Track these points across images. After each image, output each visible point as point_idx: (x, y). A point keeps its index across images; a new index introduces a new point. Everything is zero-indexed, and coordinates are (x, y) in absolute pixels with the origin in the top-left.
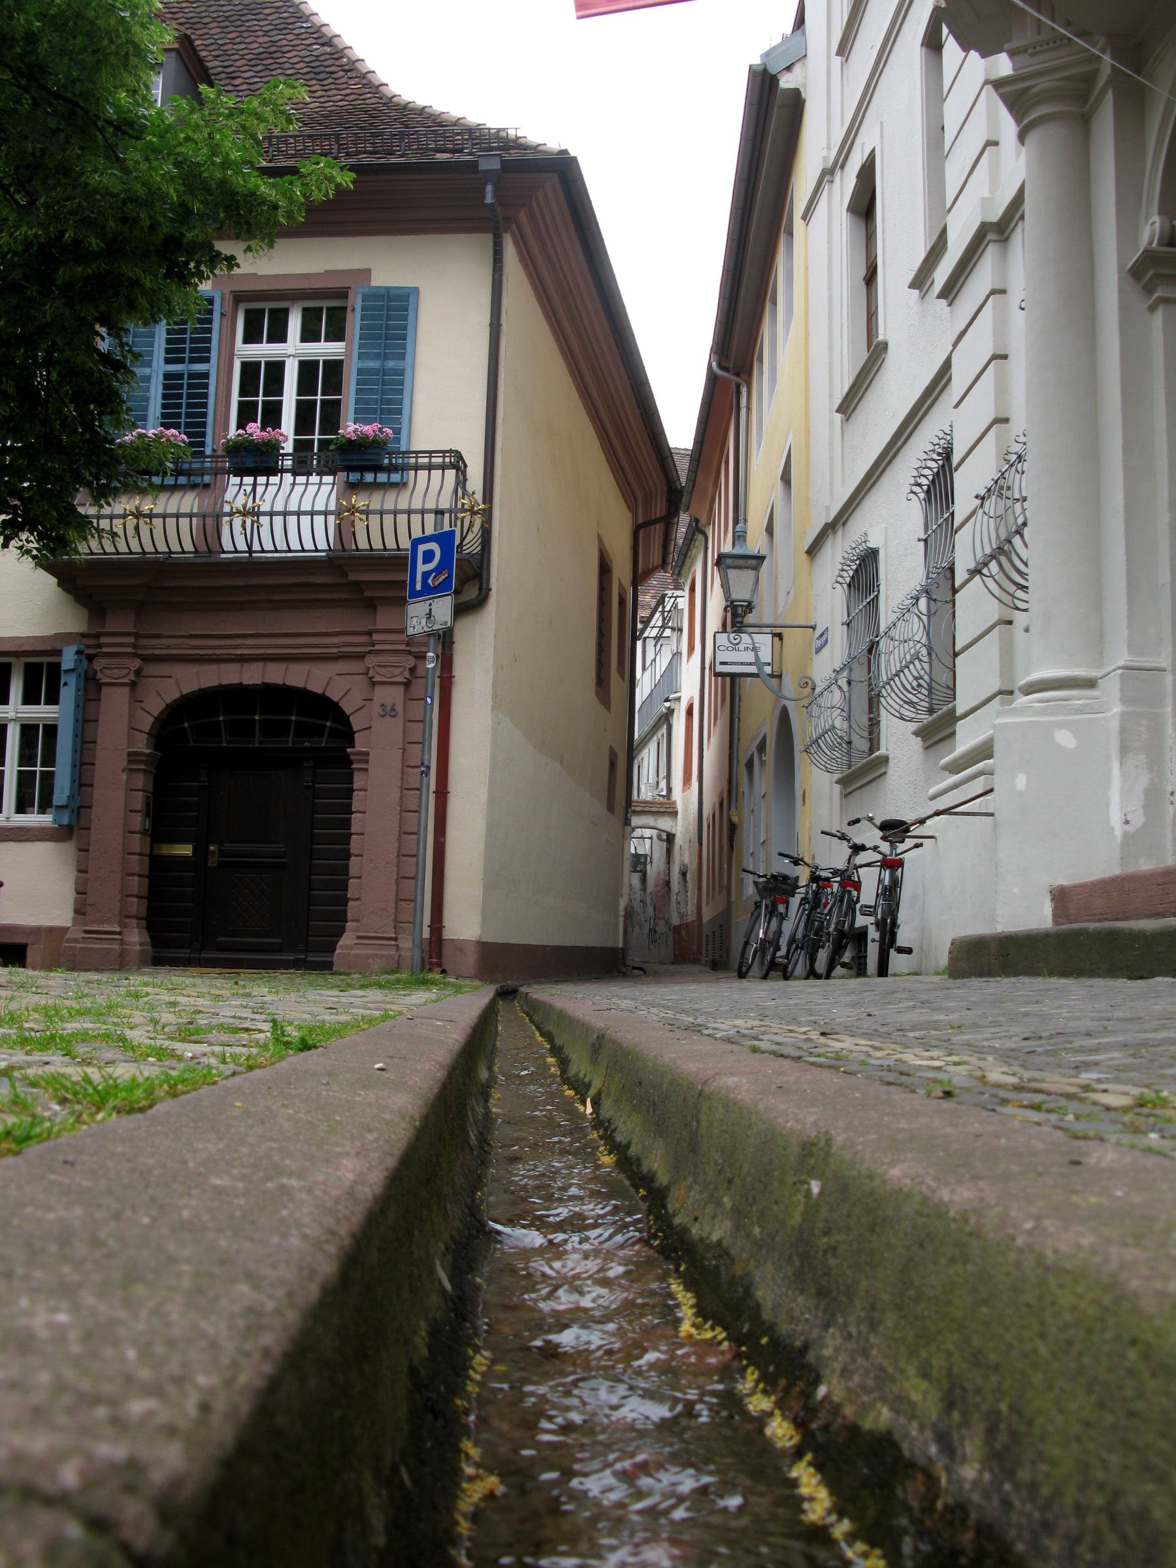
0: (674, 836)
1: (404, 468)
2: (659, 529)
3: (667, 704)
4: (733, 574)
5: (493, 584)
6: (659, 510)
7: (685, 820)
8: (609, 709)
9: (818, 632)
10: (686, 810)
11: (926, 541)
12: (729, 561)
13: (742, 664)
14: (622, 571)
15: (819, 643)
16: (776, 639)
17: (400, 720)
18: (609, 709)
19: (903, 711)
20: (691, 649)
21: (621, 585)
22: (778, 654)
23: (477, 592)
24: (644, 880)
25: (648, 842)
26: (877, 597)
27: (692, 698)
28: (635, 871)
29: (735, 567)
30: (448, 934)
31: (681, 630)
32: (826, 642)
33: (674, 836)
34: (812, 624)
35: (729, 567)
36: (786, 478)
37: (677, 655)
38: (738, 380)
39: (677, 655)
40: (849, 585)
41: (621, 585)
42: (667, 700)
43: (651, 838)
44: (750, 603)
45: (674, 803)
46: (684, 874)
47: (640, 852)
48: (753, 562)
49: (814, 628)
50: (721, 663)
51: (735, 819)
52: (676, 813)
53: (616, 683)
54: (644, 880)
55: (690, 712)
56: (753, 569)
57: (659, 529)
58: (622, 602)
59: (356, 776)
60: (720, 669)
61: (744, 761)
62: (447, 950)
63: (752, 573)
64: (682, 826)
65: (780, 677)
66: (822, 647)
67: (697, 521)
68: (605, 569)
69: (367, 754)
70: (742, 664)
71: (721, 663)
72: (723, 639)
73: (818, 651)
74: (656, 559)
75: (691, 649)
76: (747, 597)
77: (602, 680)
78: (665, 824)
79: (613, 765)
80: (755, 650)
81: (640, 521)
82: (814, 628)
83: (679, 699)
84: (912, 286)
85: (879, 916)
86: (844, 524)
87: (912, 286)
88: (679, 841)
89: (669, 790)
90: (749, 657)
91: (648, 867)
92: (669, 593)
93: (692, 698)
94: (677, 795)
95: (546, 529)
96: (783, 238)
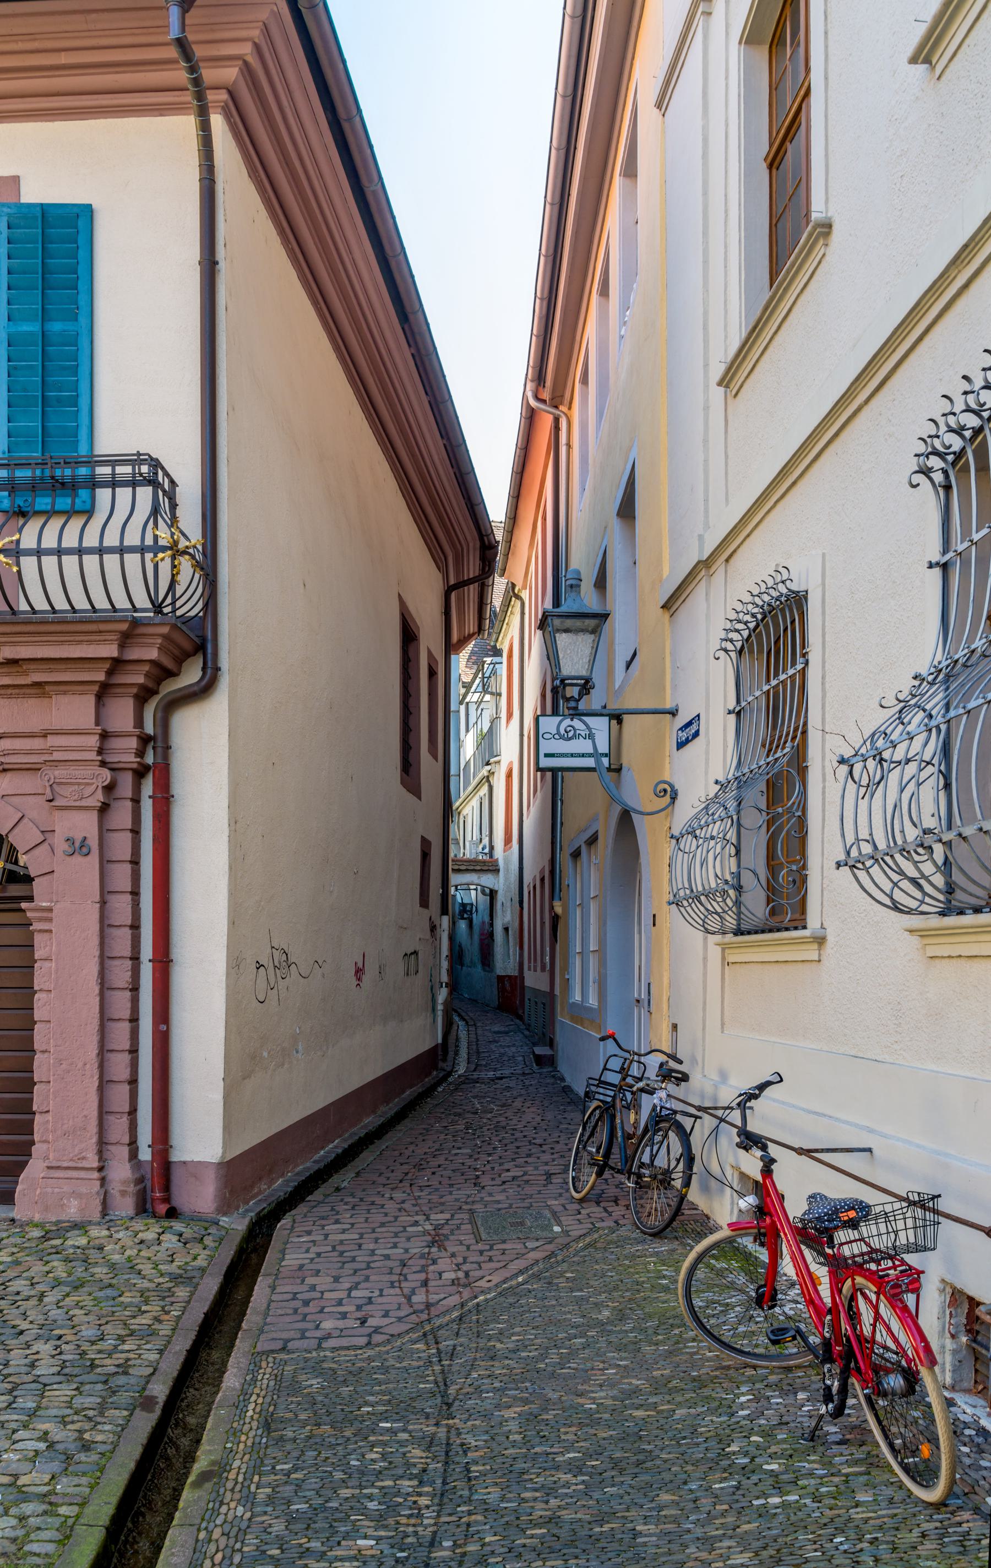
0: (496, 892)
1: (93, 484)
2: (473, 590)
3: (488, 768)
4: (563, 640)
5: (225, 661)
6: (472, 568)
7: (506, 879)
8: (420, 798)
9: (682, 719)
10: (507, 870)
11: (945, 567)
12: (557, 622)
13: (572, 755)
14: (430, 639)
15: (683, 736)
16: (614, 722)
17: (94, 858)
18: (420, 798)
19: (898, 896)
20: (510, 715)
21: (430, 654)
22: (616, 743)
23: (200, 674)
24: (470, 925)
25: (473, 893)
26: (803, 672)
27: (511, 763)
28: (463, 918)
29: (567, 631)
30: (176, 1156)
31: (500, 695)
32: (696, 734)
33: (496, 892)
34: (669, 705)
35: (558, 631)
36: (627, 510)
37: (494, 721)
38: (557, 412)
39: (494, 721)
40: (740, 652)
41: (430, 654)
42: (488, 764)
43: (476, 889)
44: (587, 680)
45: (497, 860)
46: (506, 929)
47: (465, 901)
48: (591, 623)
49: (673, 713)
50: (546, 755)
51: (558, 910)
52: (498, 870)
53: (428, 767)
54: (470, 925)
55: (509, 775)
56: (593, 632)
57: (473, 590)
58: (432, 673)
59: (38, 938)
60: (545, 762)
61: (568, 851)
62: (177, 1176)
63: (589, 638)
64: (504, 883)
65: (619, 770)
66: (687, 741)
67: (514, 586)
68: (409, 636)
69: (50, 910)
70: (572, 755)
71: (546, 755)
72: (550, 724)
73: (681, 745)
74: (472, 627)
75: (510, 715)
76: (584, 673)
77: (408, 766)
78: (487, 880)
79: (425, 856)
80: (591, 736)
81: (452, 582)
82: (673, 713)
83: (499, 762)
84: (913, 60)
85: (849, 1281)
86: (727, 561)
87: (913, 60)
88: (500, 898)
89: (492, 848)
90: (584, 746)
91: (474, 915)
92: (488, 660)
93: (511, 763)
94: (499, 853)
95: (297, 573)
96: (618, 183)
